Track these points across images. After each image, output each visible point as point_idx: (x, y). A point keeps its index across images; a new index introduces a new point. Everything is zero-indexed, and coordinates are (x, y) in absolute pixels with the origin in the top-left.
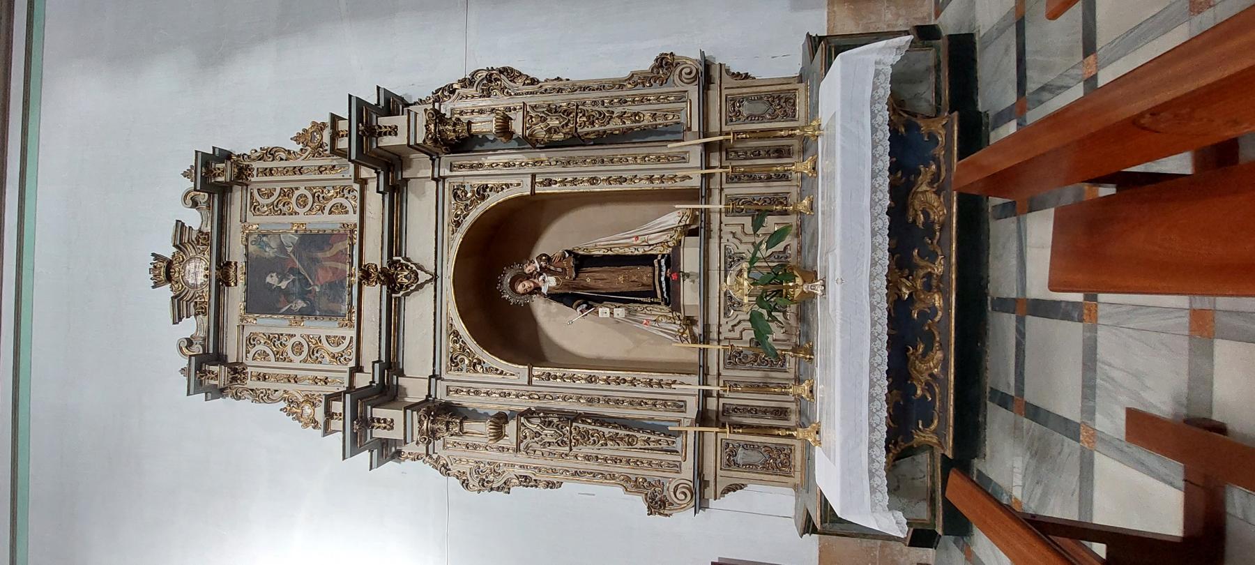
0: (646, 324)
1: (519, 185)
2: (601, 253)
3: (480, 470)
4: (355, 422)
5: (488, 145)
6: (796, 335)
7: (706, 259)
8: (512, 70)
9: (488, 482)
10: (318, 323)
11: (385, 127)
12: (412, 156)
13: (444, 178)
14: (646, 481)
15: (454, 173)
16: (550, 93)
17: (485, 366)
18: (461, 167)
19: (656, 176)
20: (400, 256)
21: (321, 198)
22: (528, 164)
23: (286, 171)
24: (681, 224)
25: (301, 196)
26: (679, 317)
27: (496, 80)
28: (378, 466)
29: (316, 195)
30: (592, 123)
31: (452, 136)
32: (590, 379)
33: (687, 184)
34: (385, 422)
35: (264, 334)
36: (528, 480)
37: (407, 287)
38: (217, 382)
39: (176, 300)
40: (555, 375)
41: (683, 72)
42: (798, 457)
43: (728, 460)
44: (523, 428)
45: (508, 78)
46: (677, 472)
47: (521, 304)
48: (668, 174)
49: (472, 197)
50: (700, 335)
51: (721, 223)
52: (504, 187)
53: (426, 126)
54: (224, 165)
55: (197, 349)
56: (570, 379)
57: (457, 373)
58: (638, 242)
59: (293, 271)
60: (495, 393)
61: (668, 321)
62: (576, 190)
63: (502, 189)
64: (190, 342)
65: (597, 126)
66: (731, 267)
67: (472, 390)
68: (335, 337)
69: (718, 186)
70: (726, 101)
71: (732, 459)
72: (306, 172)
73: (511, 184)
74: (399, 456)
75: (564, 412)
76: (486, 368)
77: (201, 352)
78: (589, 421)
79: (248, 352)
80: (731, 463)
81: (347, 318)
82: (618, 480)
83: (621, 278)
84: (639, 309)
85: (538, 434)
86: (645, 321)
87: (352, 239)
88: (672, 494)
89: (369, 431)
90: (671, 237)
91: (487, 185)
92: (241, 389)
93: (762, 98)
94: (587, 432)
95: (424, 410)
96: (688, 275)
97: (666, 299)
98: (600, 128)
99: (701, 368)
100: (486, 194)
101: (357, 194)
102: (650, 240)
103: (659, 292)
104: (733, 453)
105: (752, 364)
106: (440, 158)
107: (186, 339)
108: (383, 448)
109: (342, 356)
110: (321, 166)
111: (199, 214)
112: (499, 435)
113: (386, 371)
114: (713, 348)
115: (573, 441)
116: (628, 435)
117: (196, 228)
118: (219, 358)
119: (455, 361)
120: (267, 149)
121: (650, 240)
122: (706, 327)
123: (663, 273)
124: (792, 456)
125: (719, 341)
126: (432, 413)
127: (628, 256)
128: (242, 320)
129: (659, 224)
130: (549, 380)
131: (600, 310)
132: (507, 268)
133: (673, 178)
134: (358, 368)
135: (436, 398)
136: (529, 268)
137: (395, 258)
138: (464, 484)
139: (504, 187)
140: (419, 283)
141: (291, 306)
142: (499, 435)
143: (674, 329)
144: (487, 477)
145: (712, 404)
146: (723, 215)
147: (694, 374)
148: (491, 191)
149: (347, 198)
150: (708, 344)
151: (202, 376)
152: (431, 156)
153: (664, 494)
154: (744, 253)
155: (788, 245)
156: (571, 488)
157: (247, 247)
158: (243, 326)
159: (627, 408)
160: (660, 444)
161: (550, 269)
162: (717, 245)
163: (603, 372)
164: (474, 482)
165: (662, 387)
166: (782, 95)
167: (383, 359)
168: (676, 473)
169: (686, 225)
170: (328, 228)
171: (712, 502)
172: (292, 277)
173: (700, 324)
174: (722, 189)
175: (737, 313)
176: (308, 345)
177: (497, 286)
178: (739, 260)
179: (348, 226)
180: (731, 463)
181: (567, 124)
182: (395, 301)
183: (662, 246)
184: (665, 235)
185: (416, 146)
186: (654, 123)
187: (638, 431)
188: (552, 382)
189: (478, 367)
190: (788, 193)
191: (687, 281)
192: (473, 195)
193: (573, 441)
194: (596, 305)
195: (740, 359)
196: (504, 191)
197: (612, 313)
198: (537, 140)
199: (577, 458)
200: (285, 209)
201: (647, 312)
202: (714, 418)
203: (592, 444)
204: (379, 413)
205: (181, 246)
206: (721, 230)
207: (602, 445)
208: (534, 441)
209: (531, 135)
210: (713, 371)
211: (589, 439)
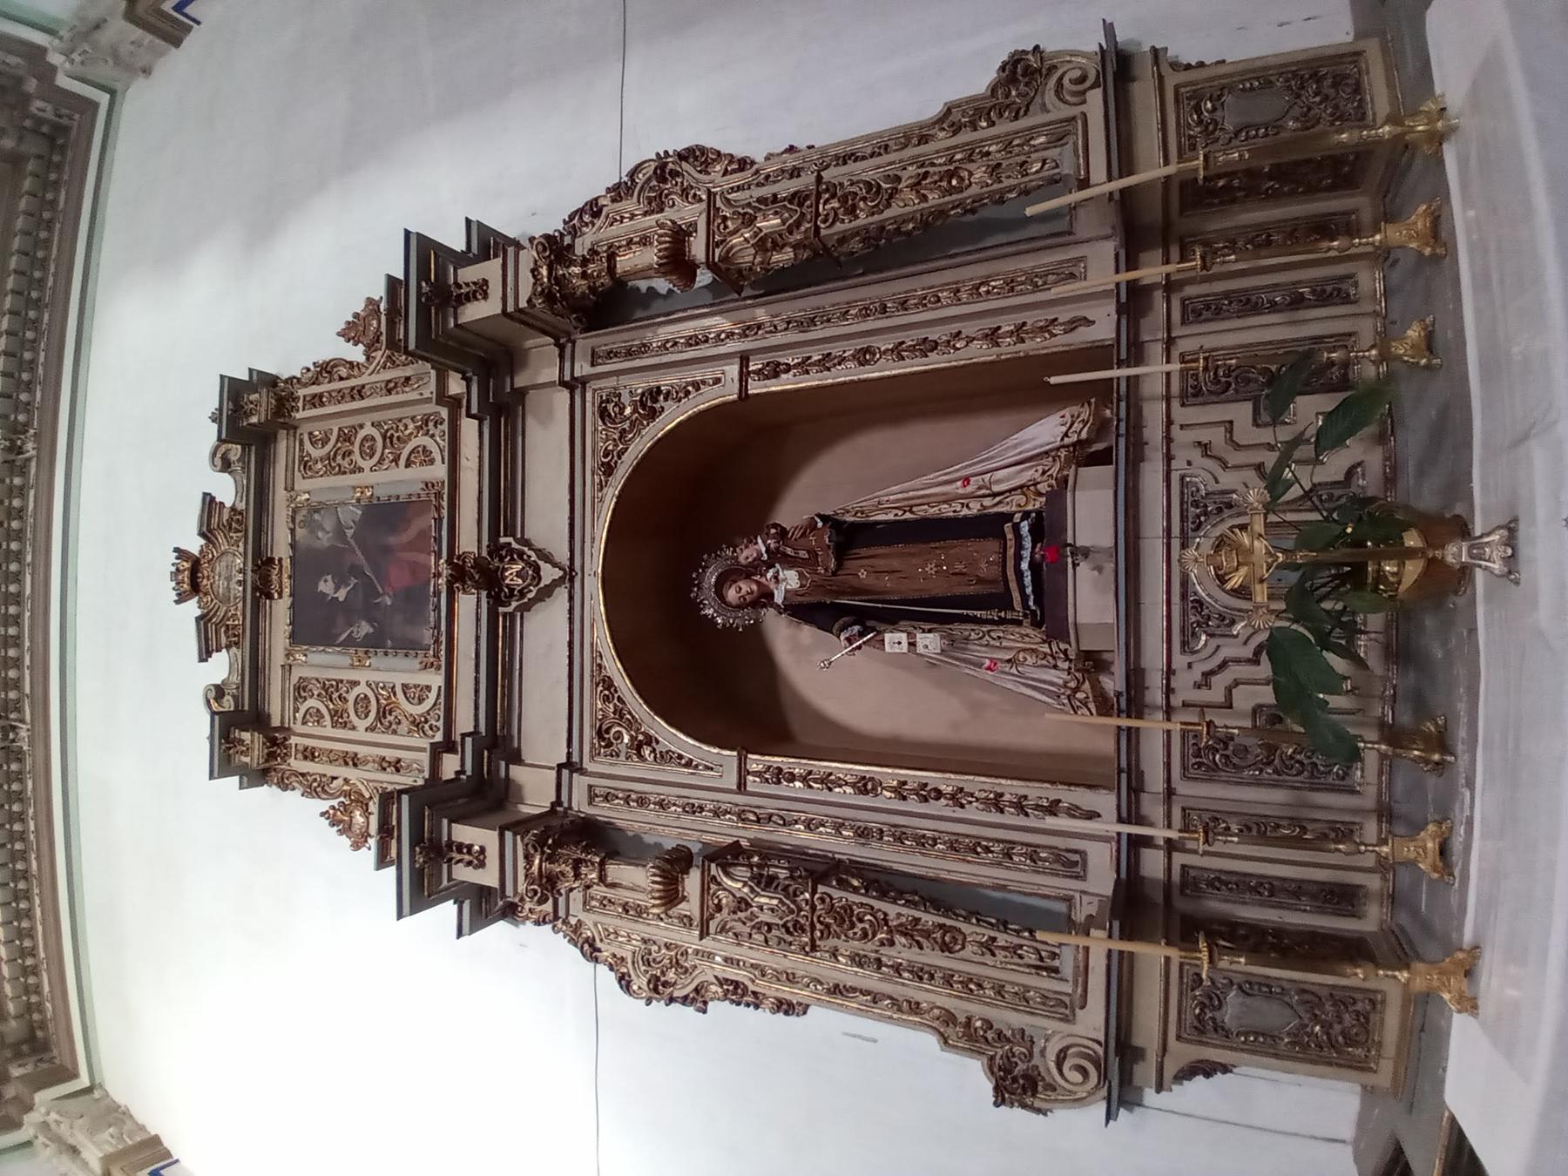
0: (989, 668)
1: (717, 381)
2: (890, 517)
3: (651, 958)
4: (417, 849)
5: (659, 305)
6: (1382, 698)
7: (1131, 512)
8: (703, 150)
9: (665, 984)
10: (391, 661)
11: (467, 285)
12: (529, 343)
13: (583, 382)
14: (991, 1027)
15: (600, 369)
16: (774, 182)
17: (658, 749)
18: (611, 354)
19: (1005, 329)
20: (513, 535)
21: (395, 440)
22: (733, 334)
23: (341, 396)
24: (1067, 441)
25: (365, 439)
26: (1065, 652)
27: (674, 174)
28: (472, 931)
29: (388, 434)
30: (852, 211)
31: (581, 285)
32: (864, 786)
33: (1084, 336)
34: (469, 852)
35: (317, 680)
36: (739, 991)
37: (522, 594)
38: (247, 760)
39: (202, 623)
40: (791, 774)
41: (1066, 81)
42: (1391, 1021)
43: (1198, 1017)
44: (714, 887)
45: (695, 167)
46: (1065, 1019)
47: (737, 628)
48: (1032, 318)
49: (632, 413)
50: (1118, 695)
51: (1169, 422)
52: (690, 388)
53: (533, 271)
54: (257, 395)
55: (228, 704)
56: (822, 783)
57: (610, 760)
58: (969, 489)
59: (356, 571)
60: (674, 805)
61: (1039, 662)
62: (830, 381)
63: (687, 393)
64: (220, 691)
65: (862, 215)
66: (1198, 527)
67: (634, 796)
68: (416, 686)
69: (1162, 335)
70: (1177, 101)
71: (1209, 1015)
72: (368, 393)
73: (704, 382)
74: (514, 914)
75: (808, 854)
76: (661, 752)
77: (232, 709)
78: (855, 883)
79: (296, 710)
80: (1204, 1027)
81: (431, 652)
82: (926, 1016)
83: (930, 569)
84: (973, 636)
85: (742, 904)
86: (987, 662)
87: (438, 508)
88: (1052, 1065)
89: (445, 866)
90: (1044, 473)
91: (658, 388)
92: (288, 773)
93: (1271, 82)
94: (848, 908)
95: (534, 835)
96: (1086, 553)
97: (1033, 612)
98: (871, 219)
99: (1124, 776)
100: (657, 406)
101: (445, 427)
102: (999, 482)
103: (1016, 595)
104: (1213, 1000)
105: (1261, 771)
106: (574, 343)
107: (214, 685)
108: (481, 898)
109: (426, 721)
110: (390, 381)
111: (232, 481)
112: (671, 895)
113: (486, 753)
114: (1153, 728)
115: (818, 926)
116: (942, 926)
117: (228, 504)
118: (256, 718)
119: (607, 736)
120: (321, 366)
121: (999, 482)
122: (1135, 677)
123: (1026, 554)
124: (1374, 1018)
125: (1169, 711)
126: (550, 841)
127: (948, 519)
128: (287, 656)
129: (1016, 446)
130: (779, 782)
131: (888, 637)
132: (709, 555)
133: (1046, 328)
134: (448, 746)
135: (570, 808)
136: (746, 553)
137: (503, 540)
138: (623, 982)
139: (690, 388)
140: (542, 585)
141: (352, 632)
142: (671, 895)
143: (1056, 680)
144: (663, 973)
145: (1153, 864)
146: (1175, 404)
147: (1104, 788)
148: (666, 399)
149: (432, 436)
150: (1140, 716)
151: (230, 748)
152: (557, 339)
153: (1034, 1062)
154: (1234, 491)
155: (1359, 464)
156: (823, 1019)
157: (293, 531)
158: (290, 666)
159: (944, 858)
160: (1021, 957)
161: (785, 555)
162: (1160, 476)
163: (890, 771)
164: (640, 982)
165: (1027, 815)
166: (1324, 71)
167: (482, 728)
168: (1061, 1020)
169: (1079, 442)
170: (403, 492)
171: (1150, 1096)
172: (353, 581)
173: (1119, 668)
174: (1170, 342)
175: (1214, 642)
176: (378, 700)
177: (692, 591)
178: (1220, 510)
179: (433, 486)
180: (1204, 1027)
181: (798, 224)
182: (504, 621)
183: (1024, 494)
184: (1031, 467)
185: (518, 315)
186: (995, 186)
187: (967, 919)
188: (784, 789)
189: (646, 751)
190: (1350, 335)
191: (1084, 569)
192: (635, 411)
193: (818, 926)
194: (881, 627)
195: (1227, 757)
196: (691, 397)
197: (912, 645)
198: (740, 271)
199: (836, 957)
200: (345, 463)
201: (992, 642)
202: (1159, 898)
203: (859, 940)
204: (465, 833)
205: (209, 535)
206: (1168, 439)
207: (882, 944)
208: (736, 917)
209: (726, 258)
210: (1155, 780)
211: (853, 926)
